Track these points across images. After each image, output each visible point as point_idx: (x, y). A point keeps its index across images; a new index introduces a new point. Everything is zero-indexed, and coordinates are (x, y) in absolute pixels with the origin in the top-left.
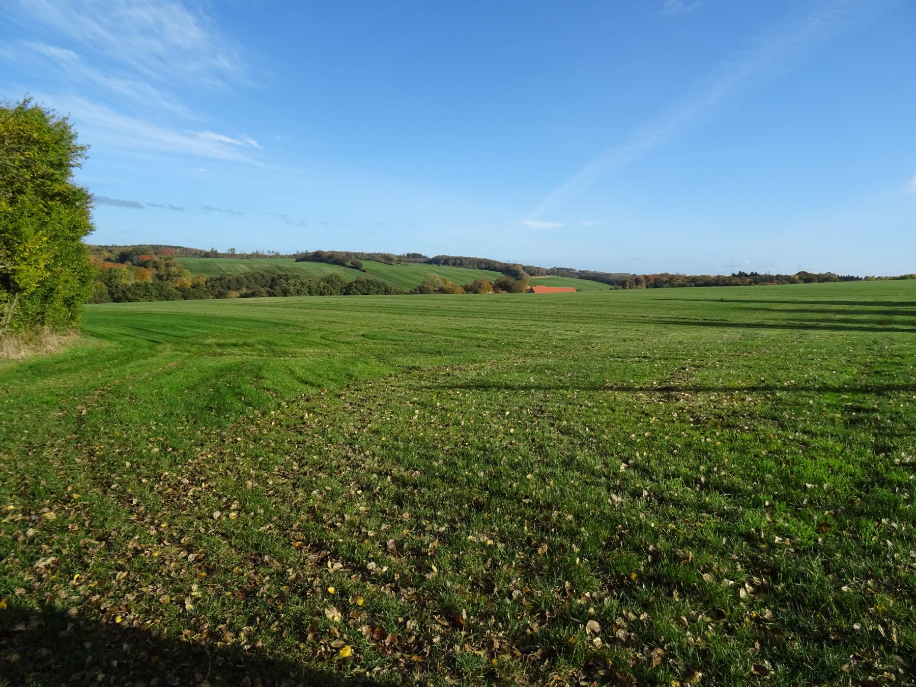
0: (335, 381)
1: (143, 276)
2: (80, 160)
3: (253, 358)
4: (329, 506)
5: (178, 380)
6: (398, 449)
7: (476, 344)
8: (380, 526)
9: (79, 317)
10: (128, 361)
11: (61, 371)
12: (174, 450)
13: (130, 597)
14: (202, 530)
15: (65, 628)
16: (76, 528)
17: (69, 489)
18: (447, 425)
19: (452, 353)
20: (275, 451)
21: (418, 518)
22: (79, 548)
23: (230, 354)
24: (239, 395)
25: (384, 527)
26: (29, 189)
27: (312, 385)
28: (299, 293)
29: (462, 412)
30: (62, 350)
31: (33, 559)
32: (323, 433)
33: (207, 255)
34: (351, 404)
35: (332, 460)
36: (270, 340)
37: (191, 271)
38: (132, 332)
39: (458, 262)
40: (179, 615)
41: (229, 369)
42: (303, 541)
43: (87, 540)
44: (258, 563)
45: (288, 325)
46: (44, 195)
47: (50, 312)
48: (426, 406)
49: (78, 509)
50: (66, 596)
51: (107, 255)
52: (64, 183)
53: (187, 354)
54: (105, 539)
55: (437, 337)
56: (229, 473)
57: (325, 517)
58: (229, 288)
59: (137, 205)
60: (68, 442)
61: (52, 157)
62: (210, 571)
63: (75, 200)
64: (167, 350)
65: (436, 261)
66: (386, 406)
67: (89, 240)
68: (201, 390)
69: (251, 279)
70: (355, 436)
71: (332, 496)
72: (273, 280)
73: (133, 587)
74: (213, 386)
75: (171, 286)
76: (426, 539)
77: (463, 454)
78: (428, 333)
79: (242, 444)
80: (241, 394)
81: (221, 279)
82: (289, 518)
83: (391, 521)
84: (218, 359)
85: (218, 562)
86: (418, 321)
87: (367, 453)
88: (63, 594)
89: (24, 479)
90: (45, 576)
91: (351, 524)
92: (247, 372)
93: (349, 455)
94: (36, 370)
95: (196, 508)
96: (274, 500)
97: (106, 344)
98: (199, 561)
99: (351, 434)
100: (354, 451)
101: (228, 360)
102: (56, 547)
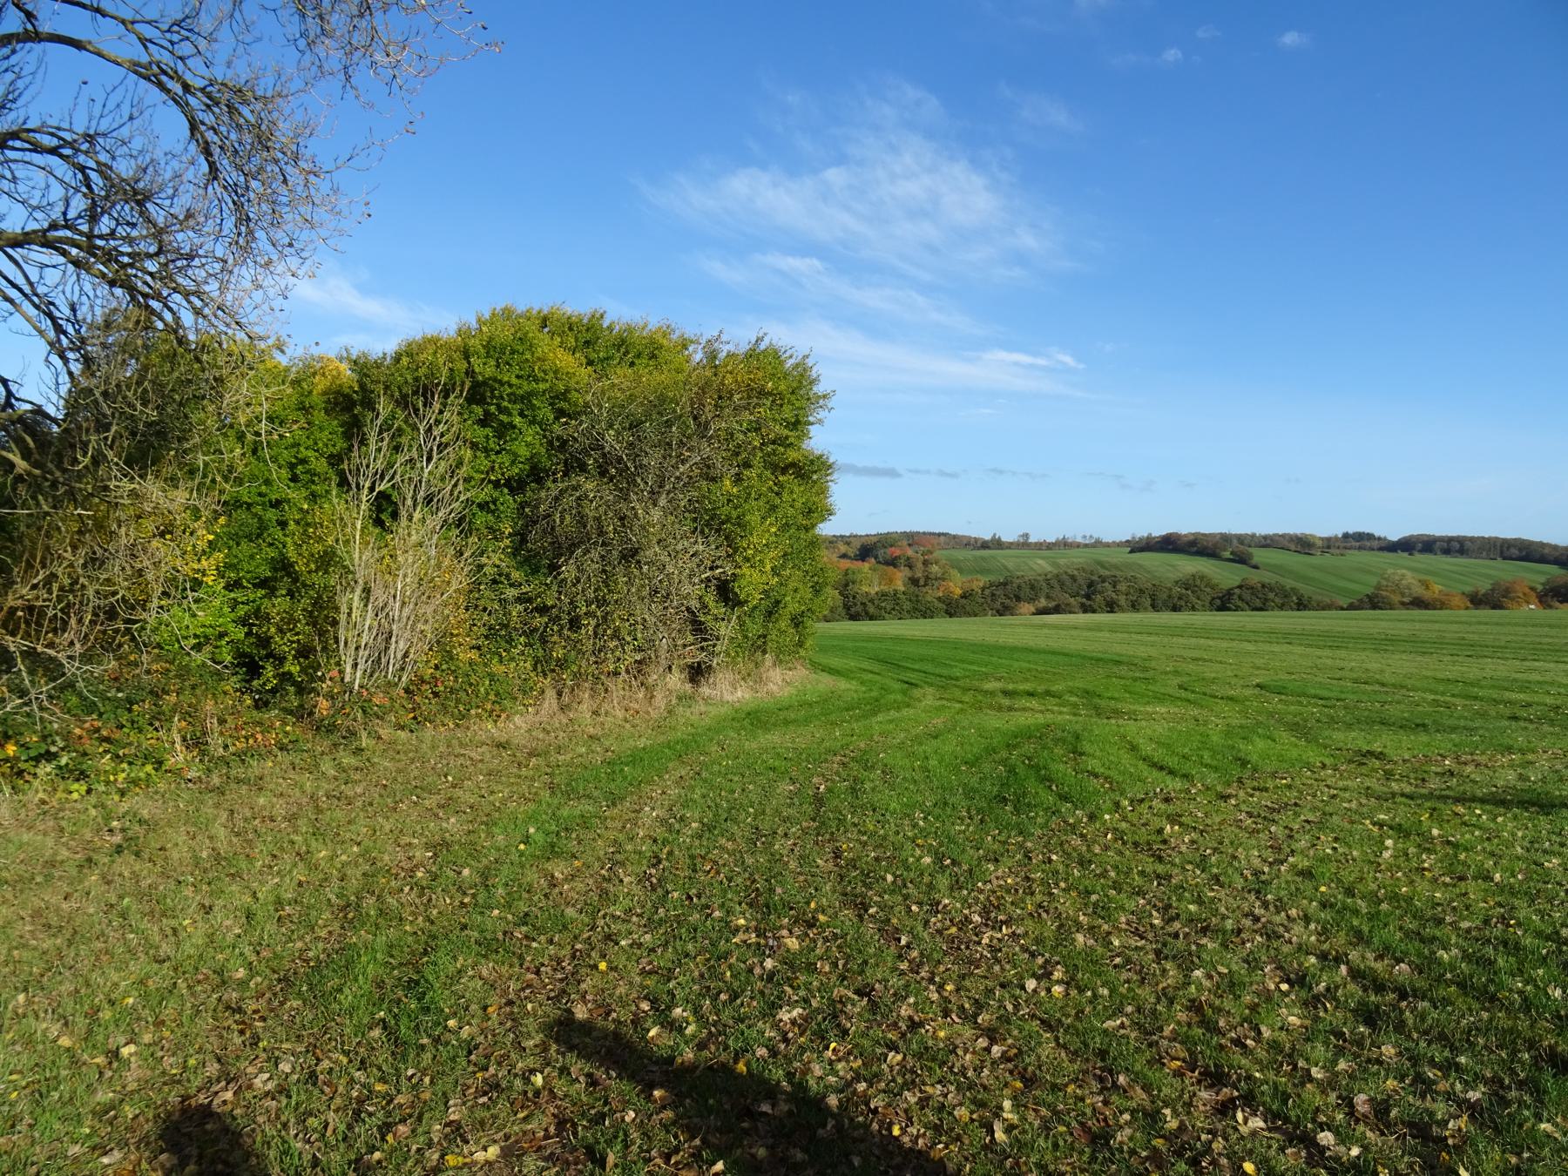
0: (1216, 769)
1: (891, 581)
2: (822, 414)
3: (1064, 717)
4: (1228, 1004)
5: (948, 748)
6: (1356, 912)
7: (1508, 712)
8: (1335, 1062)
9: (809, 643)
10: (875, 714)
11: (786, 722)
12: (954, 862)
13: (911, 1098)
14: (1010, 1008)
15: (824, 1126)
16: (827, 969)
17: (813, 905)
18: (1462, 878)
19: (1454, 729)
20: (1116, 886)
21: (1415, 1060)
22: (832, 1002)
23: (1024, 709)
24: (1047, 780)
25: (1342, 1065)
26: (757, 461)
27: (1171, 772)
28: (1135, 607)
29: (1492, 854)
30: (788, 691)
31: (774, 1007)
32: (1203, 864)
33: (985, 545)
34: (1250, 814)
35: (1224, 917)
36: (1090, 688)
37: (961, 571)
38: (876, 667)
39: (1456, 547)
40: (985, 1147)
41: (1026, 734)
42: (1184, 1061)
43: (844, 991)
44: (1108, 1087)
45: (1118, 663)
46: (774, 468)
47: (773, 635)
48: (1407, 835)
49: (826, 940)
50: (825, 1071)
51: (843, 548)
52: (362, 386)
53: (958, 706)
54: (868, 995)
55: (1417, 696)
56: (1044, 915)
57: (1222, 1023)
58: (1018, 599)
59: (891, 473)
60: (805, 831)
61: (788, 413)
62: (1030, 1082)
63: (811, 472)
64: (928, 697)
65: (1406, 546)
66: (1321, 825)
67: (826, 529)
68: (987, 767)
69: (1054, 582)
70: (1263, 878)
71: (1232, 985)
72: (1091, 584)
73: (913, 1082)
74: (1004, 762)
75: (931, 595)
76: (1440, 1109)
77: (1505, 944)
78: (1394, 686)
79: (1061, 868)
80: (1051, 780)
81: (1005, 584)
82: (1154, 1012)
83: (1356, 1056)
84: (1006, 716)
85: (1040, 1067)
86: (1373, 663)
87: (1293, 912)
88: (817, 1070)
89: (754, 881)
90: (790, 1035)
91: (1274, 1046)
92: (1057, 741)
93: (1257, 911)
94: (755, 719)
95: (997, 968)
96: (1124, 976)
97: (843, 684)
98: (1009, 1060)
99: (1256, 873)
100: (1265, 905)
101: (1022, 720)
102: (802, 993)
